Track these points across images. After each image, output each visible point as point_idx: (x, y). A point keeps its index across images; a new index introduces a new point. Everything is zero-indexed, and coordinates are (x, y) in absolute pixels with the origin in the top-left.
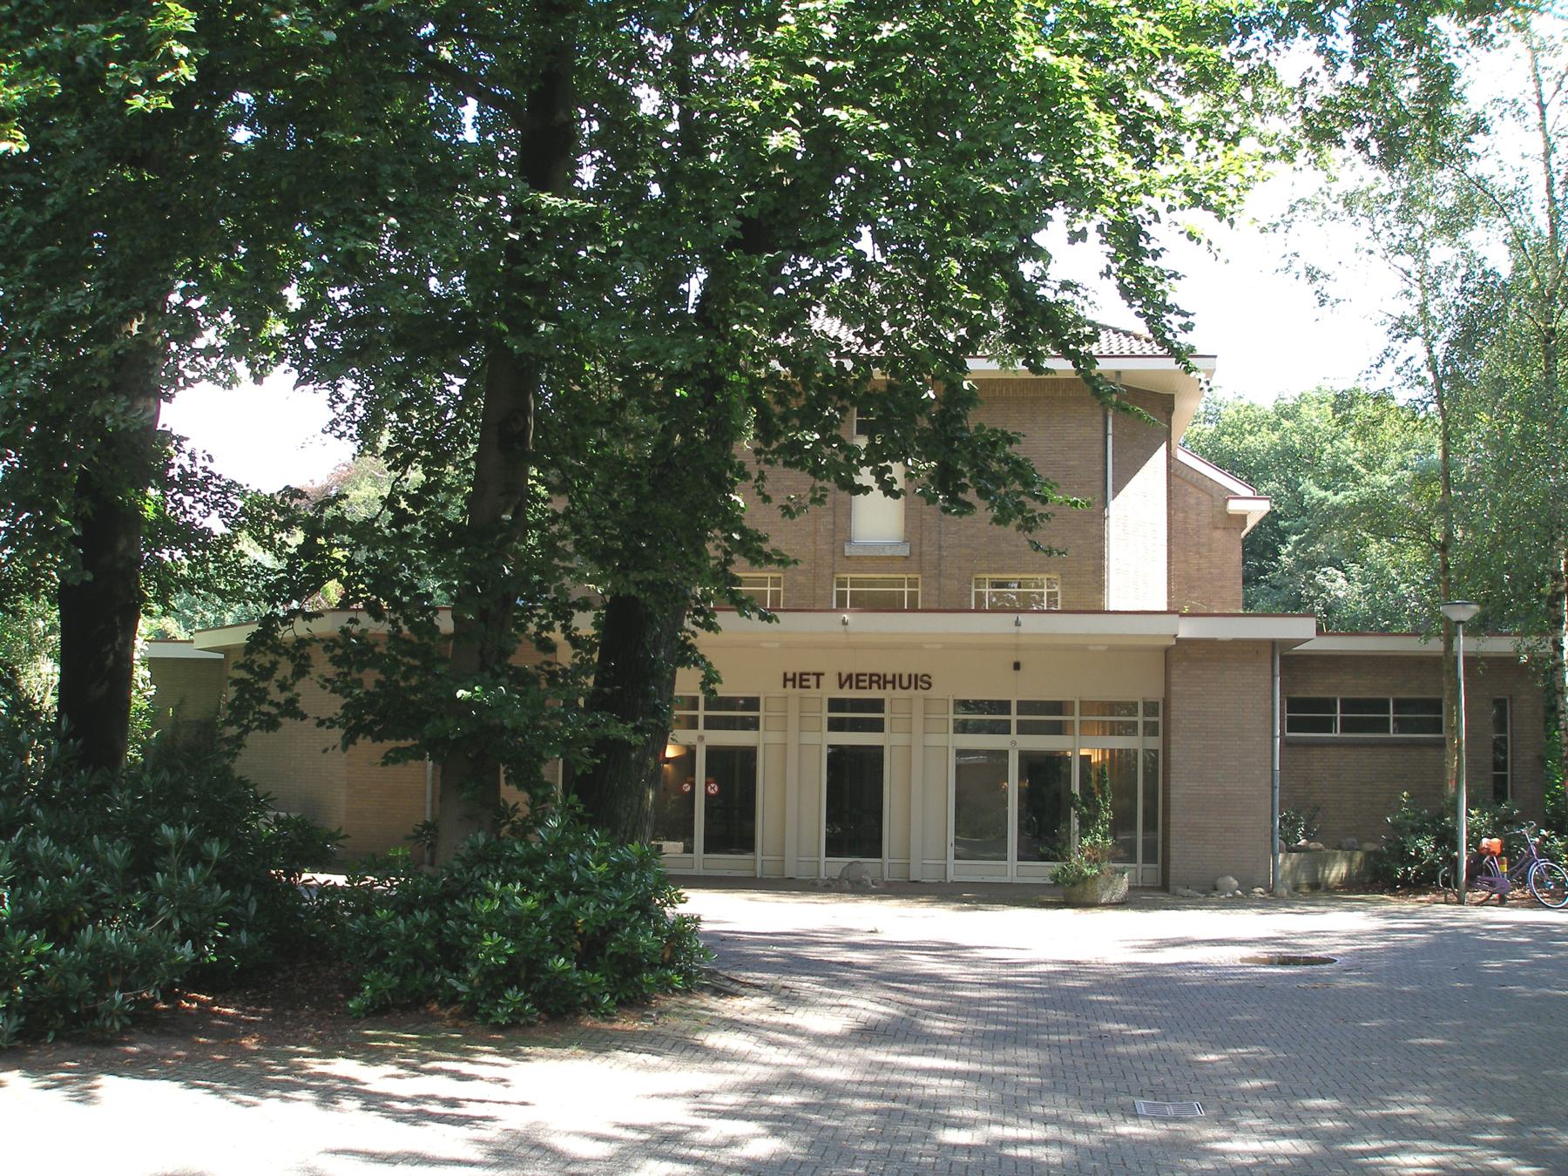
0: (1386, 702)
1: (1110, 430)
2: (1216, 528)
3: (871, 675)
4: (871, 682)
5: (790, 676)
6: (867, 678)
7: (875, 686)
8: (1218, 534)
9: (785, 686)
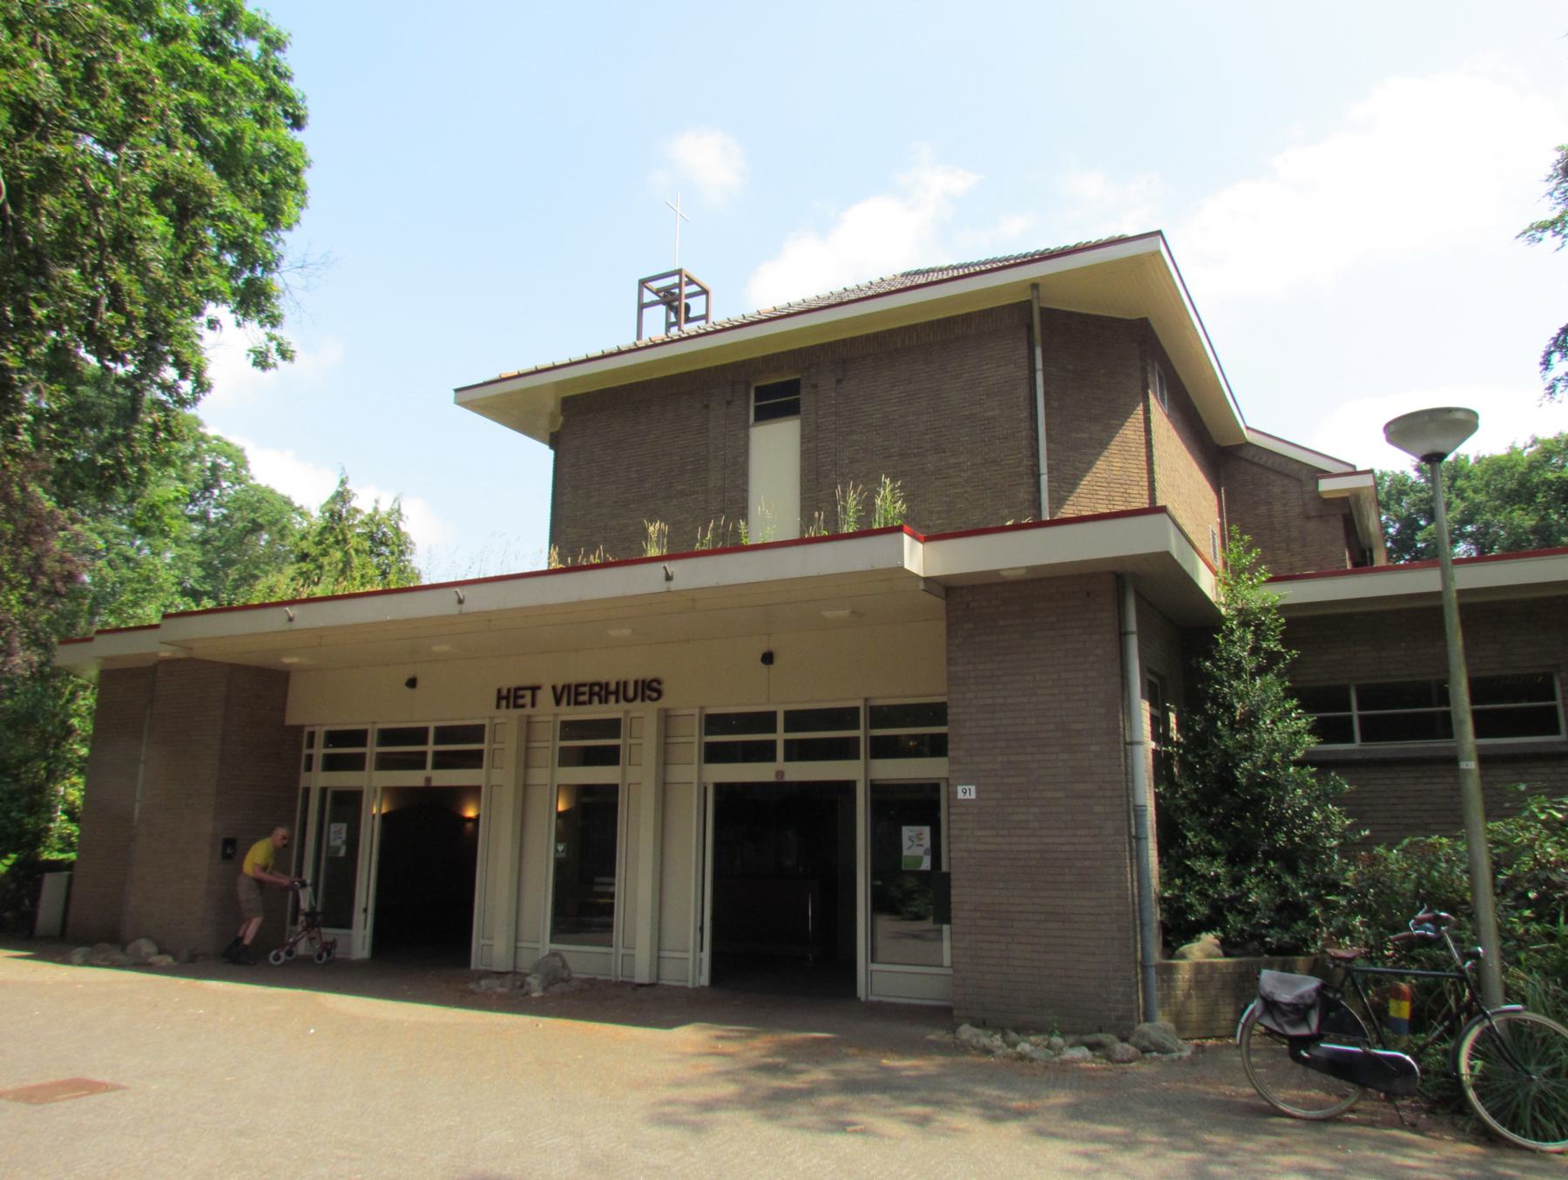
0: (1345, 690)
1: (1039, 364)
2: (1308, 518)
3: (592, 685)
4: (592, 694)
5: (504, 693)
6: (586, 689)
7: (596, 699)
8: (1312, 525)
9: (498, 706)
